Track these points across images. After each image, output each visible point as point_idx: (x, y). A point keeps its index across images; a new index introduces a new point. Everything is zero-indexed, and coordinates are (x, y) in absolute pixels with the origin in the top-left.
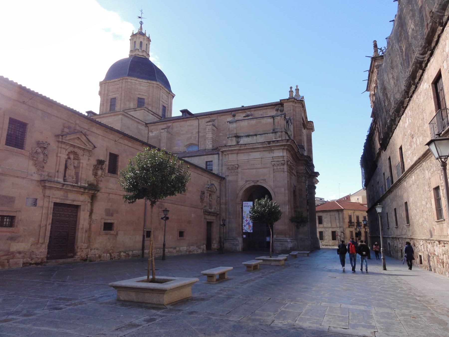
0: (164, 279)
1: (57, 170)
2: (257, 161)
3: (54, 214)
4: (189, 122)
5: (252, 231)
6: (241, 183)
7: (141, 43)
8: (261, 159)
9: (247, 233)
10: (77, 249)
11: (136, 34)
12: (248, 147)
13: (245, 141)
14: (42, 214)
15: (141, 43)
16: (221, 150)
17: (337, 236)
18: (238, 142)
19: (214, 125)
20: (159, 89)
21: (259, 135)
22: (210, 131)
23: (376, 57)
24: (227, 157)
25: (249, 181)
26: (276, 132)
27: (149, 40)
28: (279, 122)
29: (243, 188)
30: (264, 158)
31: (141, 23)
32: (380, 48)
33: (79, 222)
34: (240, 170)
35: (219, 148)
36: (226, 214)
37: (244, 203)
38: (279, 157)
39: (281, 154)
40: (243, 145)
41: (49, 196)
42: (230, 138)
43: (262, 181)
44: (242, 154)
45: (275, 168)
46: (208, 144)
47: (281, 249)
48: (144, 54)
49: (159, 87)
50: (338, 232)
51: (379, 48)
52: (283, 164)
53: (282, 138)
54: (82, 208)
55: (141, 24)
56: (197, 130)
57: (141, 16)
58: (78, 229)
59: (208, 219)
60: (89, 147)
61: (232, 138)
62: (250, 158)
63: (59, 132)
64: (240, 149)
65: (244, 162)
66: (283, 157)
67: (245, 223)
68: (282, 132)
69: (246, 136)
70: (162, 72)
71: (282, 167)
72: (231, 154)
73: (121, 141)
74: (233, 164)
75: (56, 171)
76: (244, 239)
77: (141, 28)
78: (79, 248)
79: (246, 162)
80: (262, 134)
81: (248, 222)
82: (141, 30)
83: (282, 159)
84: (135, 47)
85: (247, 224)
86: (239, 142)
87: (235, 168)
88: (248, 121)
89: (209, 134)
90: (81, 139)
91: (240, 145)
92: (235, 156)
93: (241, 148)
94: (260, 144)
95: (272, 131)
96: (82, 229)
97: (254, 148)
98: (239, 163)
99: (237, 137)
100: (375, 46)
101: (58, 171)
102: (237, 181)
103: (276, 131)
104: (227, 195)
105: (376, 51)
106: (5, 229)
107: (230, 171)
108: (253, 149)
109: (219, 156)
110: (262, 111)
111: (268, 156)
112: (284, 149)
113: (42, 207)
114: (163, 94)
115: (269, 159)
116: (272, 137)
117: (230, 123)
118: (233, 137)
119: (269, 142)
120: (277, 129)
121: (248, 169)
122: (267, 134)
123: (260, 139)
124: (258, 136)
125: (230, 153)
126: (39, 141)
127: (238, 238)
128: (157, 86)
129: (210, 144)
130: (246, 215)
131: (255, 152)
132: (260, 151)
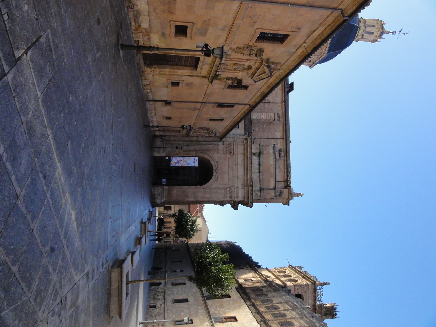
0: (128, 287)
1: (233, 59)
2: (235, 173)
4: (281, 93)
5: (171, 165)
7: (372, 33)
8: (237, 176)
9: (169, 160)
10: (153, 68)
12: (249, 165)
13: (255, 161)
15: (372, 33)
16: (248, 139)
17: (167, 211)
18: (254, 154)
19: (274, 120)
21: (259, 175)
22: (269, 117)
23: (315, 285)
24: (242, 143)
26: (260, 191)
27: (374, 41)
28: (269, 195)
30: (238, 179)
31: (394, 33)
32: (322, 287)
34: (228, 156)
35: (250, 137)
36: (187, 141)
37: (198, 158)
38: (237, 194)
39: (240, 195)
40: (251, 160)
42: (259, 147)
43: (216, 177)
44: (243, 159)
45: (228, 190)
46: (256, 114)
47: (155, 194)
48: (359, 37)
49: (322, 55)
50: (171, 212)
51: (322, 286)
52: (231, 197)
53: (255, 196)
55: (392, 33)
57: (401, 33)
58: (173, 69)
61: (259, 149)
62: (239, 166)
63: (271, 60)
64: (248, 157)
66: (237, 197)
67: (179, 158)
68: (260, 196)
69: (260, 163)
71: (228, 196)
72: (244, 148)
73: (260, 93)
74: (235, 149)
75: (232, 59)
76: (165, 157)
77: (388, 32)
78: (154, 69)
80: (260, 178)
81: (180, 161)
82: (386, 32)
83: (235, 196)
84: (369, 26)
85: (178, 161)
86: (254, 156)
87: (230, 151)
89: (267, 116)
92: (242, 151)
93: (248, 158)
94: (251, 177)
95: (262, 187)
97: (247, 170)
98: (235, 155)
99: (260, 154)
100: (325, 284)
101: (231, 60)
102: (218, 153)
103: (262, 191)
104: (205, 143)
105: (320, 284)
107: (228, 146)
108: (247, 170)
110: (283, 167)
111: (239, 183)
112: (245, 198)
115: (237, 184)
116: (256, 187)
117: (273, 146)
118: (260, 150)
119: (252, 186)
120: (263, 192)
121: (229, 164)
122: (260, 183)
123: (256, 176)
124: (259, 174)
125: (245, 147)
126: (263, 51)
127: (165, 153)
128: (322, 53)
130: (186, 159)
131: (244, 172)
132: (244, 175)
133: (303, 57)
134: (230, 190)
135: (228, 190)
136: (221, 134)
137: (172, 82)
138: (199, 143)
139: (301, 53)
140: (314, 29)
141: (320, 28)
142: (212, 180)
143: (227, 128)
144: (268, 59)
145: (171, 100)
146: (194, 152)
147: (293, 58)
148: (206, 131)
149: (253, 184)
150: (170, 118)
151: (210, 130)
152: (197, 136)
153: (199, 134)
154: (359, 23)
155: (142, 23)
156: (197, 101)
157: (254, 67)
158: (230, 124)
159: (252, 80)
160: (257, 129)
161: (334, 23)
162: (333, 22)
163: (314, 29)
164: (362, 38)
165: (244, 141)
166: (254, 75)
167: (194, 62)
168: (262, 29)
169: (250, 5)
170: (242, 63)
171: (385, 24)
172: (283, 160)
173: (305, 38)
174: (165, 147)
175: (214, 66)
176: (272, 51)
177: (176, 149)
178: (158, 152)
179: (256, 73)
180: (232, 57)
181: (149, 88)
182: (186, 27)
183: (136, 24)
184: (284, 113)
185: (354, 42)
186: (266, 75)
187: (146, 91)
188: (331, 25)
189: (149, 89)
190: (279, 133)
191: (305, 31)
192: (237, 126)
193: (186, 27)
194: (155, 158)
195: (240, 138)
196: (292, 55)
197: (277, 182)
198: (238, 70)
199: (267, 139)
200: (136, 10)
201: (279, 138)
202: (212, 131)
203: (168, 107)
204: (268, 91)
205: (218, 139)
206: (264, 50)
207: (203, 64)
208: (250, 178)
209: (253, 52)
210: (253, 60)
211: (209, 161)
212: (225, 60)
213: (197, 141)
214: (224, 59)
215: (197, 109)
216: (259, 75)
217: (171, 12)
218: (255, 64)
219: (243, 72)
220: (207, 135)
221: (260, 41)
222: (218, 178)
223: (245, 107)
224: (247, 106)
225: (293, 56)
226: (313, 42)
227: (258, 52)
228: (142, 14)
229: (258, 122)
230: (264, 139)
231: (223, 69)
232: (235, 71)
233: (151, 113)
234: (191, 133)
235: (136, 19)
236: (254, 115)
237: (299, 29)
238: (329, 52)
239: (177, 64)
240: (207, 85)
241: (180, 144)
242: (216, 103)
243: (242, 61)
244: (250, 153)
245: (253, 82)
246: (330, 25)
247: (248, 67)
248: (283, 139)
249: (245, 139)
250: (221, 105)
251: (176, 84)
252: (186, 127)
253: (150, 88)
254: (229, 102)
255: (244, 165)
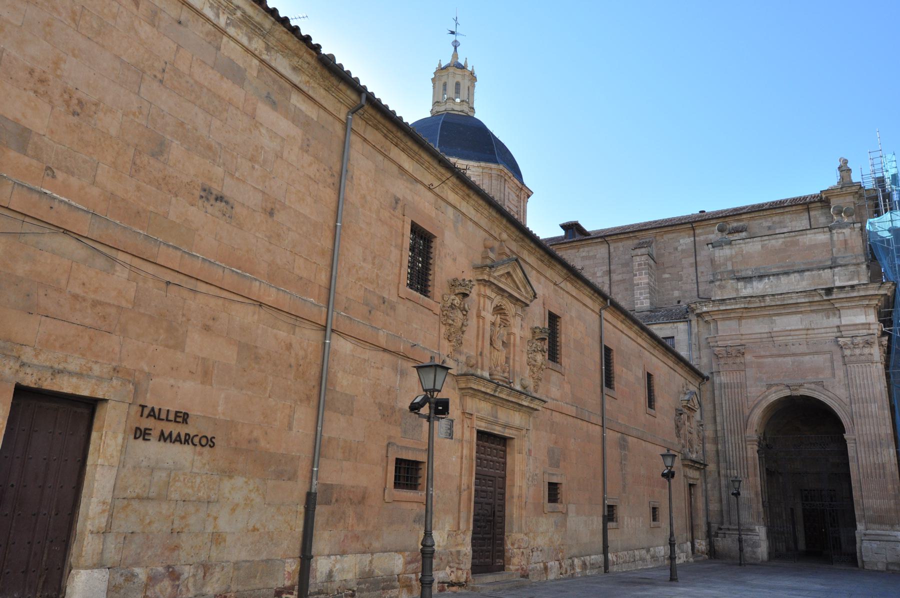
1: (480, 350)
3: (480, 462)
4: (586, 249)
6: (754, 390)
7: (458, 84)
8: (805, 332)
11: (446, 68)
14: (462, 458)
15: (458, 84)
16: (698, 311)
19: (650, 255)
20: (503, 180)
25: (777, 385)
27: (473, 77)
28: (849, 242)
29: (761, 400)
30: (814, 329)
31: (456, 45)
33: (513, 480)
34: (748, 357)
36: (718, 466)
41: (472, 415)
42: (718, 283)
43: (813, 386)
48: (465, 108)
54: (516, 443)
56: (606, 268)
59: (691, 478)
60: (522, 294)
63: (478, 261)
64: (746, 308)
65: (759, 340)
66: (867, 327)
70: (503, 144)
71: (866, 351)
72: (724, 319)
73: (568, 286)
74: (729, 343)
75: (479, 353)
79: (764, 340)
88: (761, 241)
89: (641, 274)
90: (514, 276)
91: (748, 299)
92: (733, 324)
96: (520, 496)
101: (481, 354)
104: (718, 419)
106: (412, 494)
109: (690, 324)
112: (868, 306)
113: (461, 441)
114: (510, 191)
115: (828, 330)
119: (829, 291)
121: (771, 356)
125: (721, 317)
127: (757, 528)
128: (499, 173)
129: (644, 299)
132: (801, 312)
133: (465, 188)
134: (850, 348)
135: (848, 352)
136: (690, 378)
137: (550, 501)
138: (719, 434)
139: (457, 193)
140: (395, 169)
141: (391, 155)
142: (822, 398)
143: (671, 364)
144: (476, 268)
145: (601, 507)
146: (746, 448)
147: (471, 212)
148: (683, 417)
149: (824, 287)
150: (654, 510)
151: (681, 408)
152: (703, 440)
153: (695, 436)
154: (439, 113)
155: (392, 572)
156: (600, 440)
157: (498, 300)
158: (661, 356)
159: (532, 304)
160: (676, 294)
161: (380, 126)
162: (378, 129)
163: (397, 168)
164: (468, 102)
165: (706, 322)
166: (517, 300)
167: (486, 444)
168: (399, 283)
169: (342, 313)
170: (488, 327)
171: (440, 65)
172: (751, 222)
173: (419, 186)
174: (737, 527)
175: (497, 394)
176: (455, 260)
177: (740, 497)
178: (755, 545)
179: (511, 296)
180: (473, 353)
181: (570, 561)
182: (399, 461)
183: (394, 587)
184: (631, 235)
185: (476, 116)
186: (514, 270)
187: (578, 570)
188: (385, 132)
189: (573, 561)
190: (682, 241)
191: (400, 188)
192: (668, 343)
193: (399, 461)
194: (775, 555)
195: (698, 331)
196: (463, 214)
197: (813, 227)
198: (509, 339)
199: (698, 268)
200: (358, 584)
201: (692, 239)
202: (685, 403)
203: (622, 512)
204: (559, 267)
205: (707, 385)
206: (450, 278)
207: (496, 423)
208: (805, 296)
209: (457, 301)
210: (479, 303)
211: (768, 407)
212: (482, 369)
213: (716, 441)
214: (479, 372)
215: (624, 440)
216: (518, 288)
217: (362, 499)
218: (489, 298)
219: (512, 325)
220: (697, 416)
221: (430, 289)
222: (816, 383)
223: (606, 320)
224: (606, 314)
225: (464, 210)
226: (427, 169)
227: (457, 291)
228: (367, 569)
229: (659, 292)
230: (699, 275)
231: (506, 375)
232: (512, 345)
233: (643, 559)
234: (694, 456)
235: (382, 585)
236: (642, 302)
237: (397, 203)
238: (495, 162)
239: (501, 488)
240: (553, 412)
241: (728, 487)
242: (602, 391)
243: (484, 329)
244: (736, 304)
245: (536, 300)
246: (385, 135)
247: (500, 314)
248: (694, 230)
249: (700, 319)
250: (608, 380)
251: (554, 492)
252: (667, 467)
253: (570, 558)
254: (598, 359)
255: (770, 315)
